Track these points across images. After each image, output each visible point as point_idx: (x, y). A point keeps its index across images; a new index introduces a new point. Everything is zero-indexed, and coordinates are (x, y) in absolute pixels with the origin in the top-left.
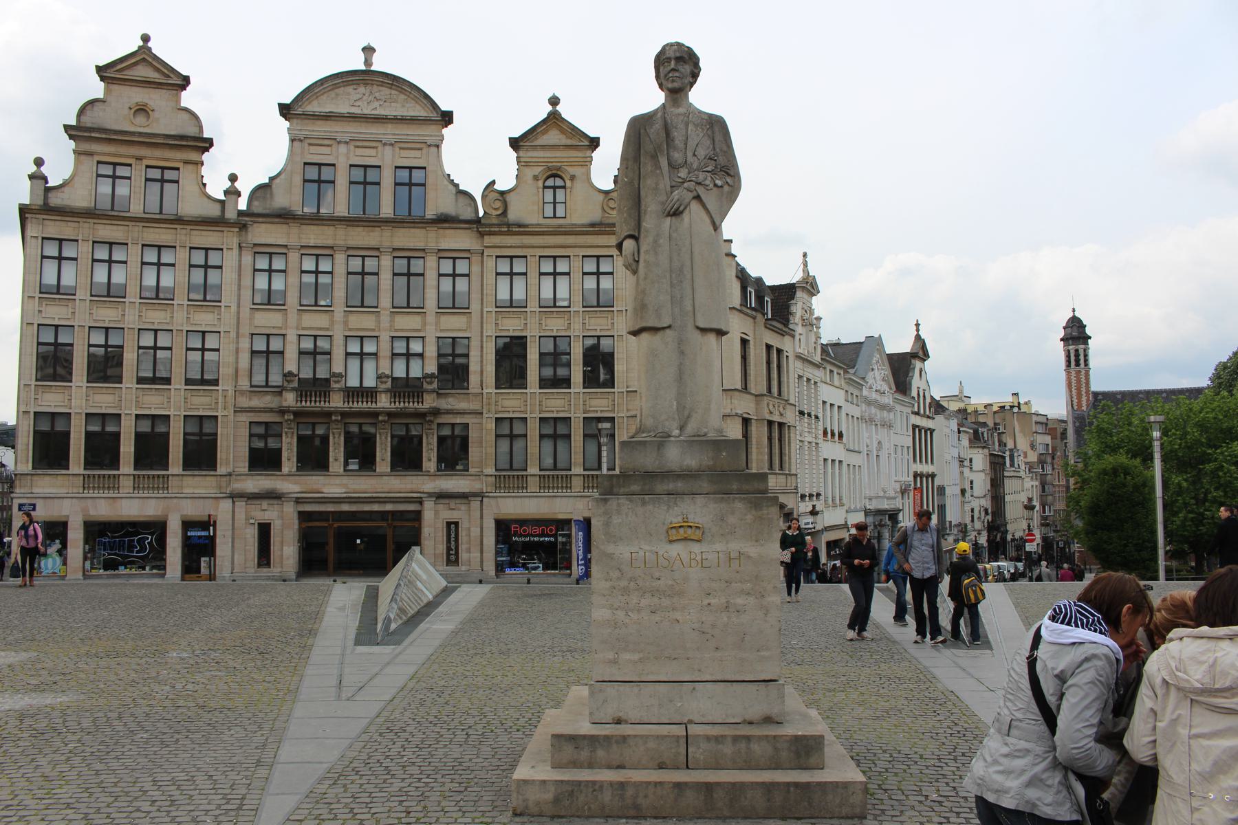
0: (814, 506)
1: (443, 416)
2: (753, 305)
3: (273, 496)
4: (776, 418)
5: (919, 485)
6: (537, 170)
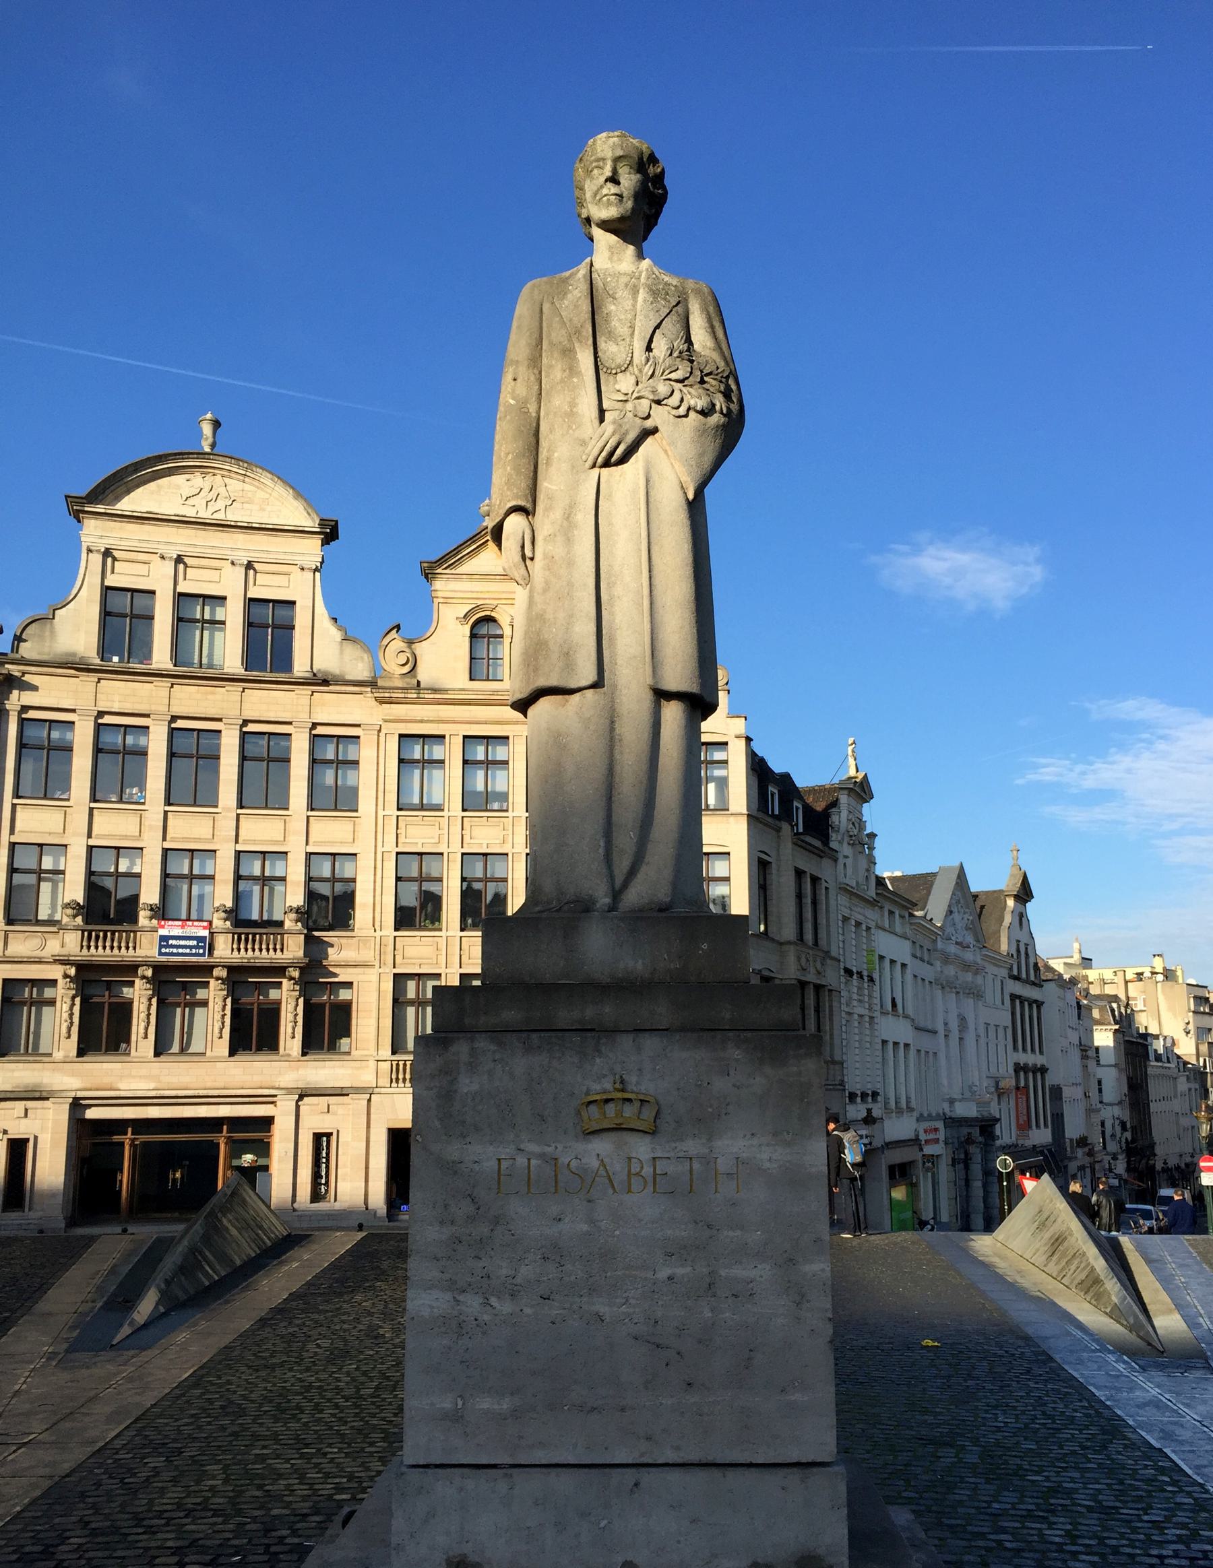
0: (869, 1111)
2: (777, 812)
4: (811, 977)
5: (1022, 1084)
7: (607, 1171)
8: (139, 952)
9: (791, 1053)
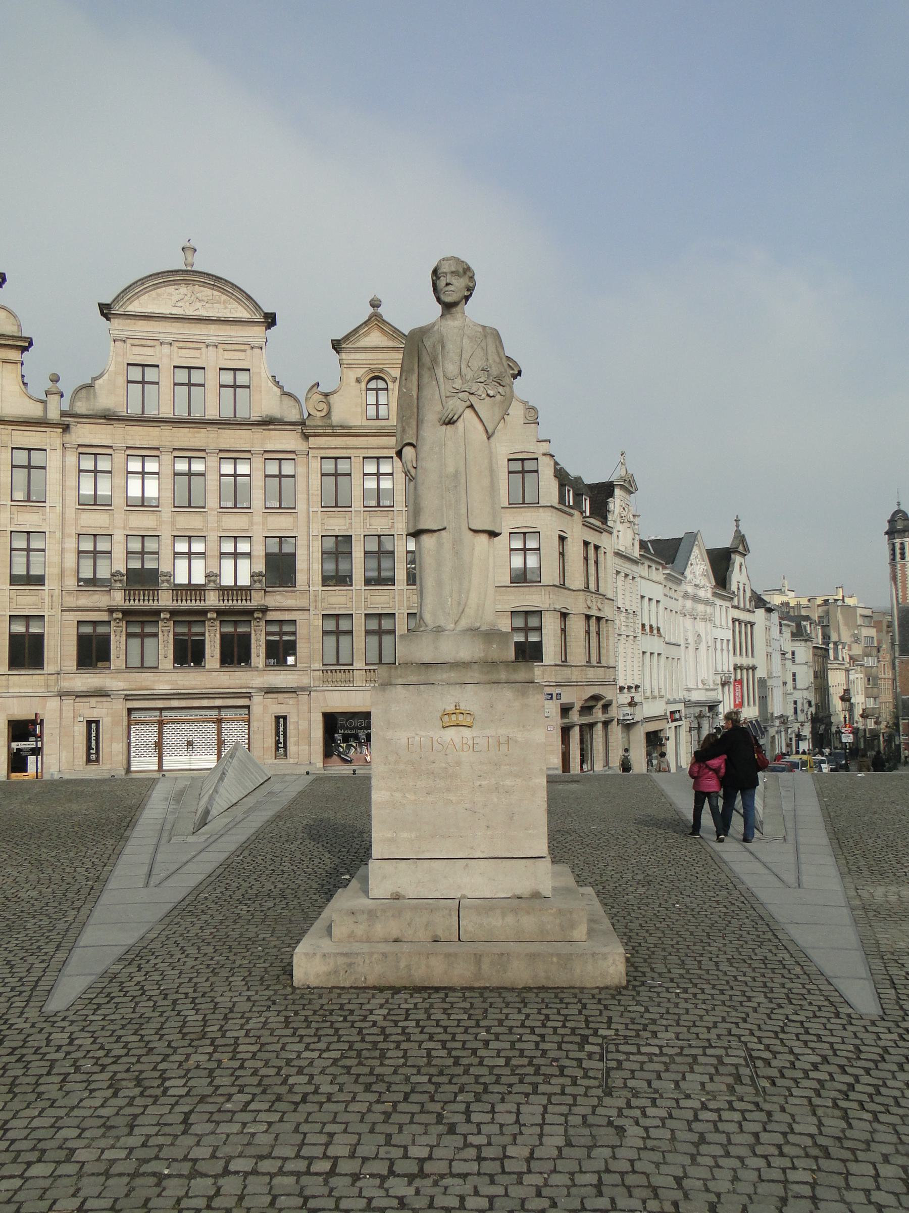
0: (632, 698)
1: (271, 613)
2: (571, 504)
3: (101, 694)
6: (360, 372)
8: (161, 603)
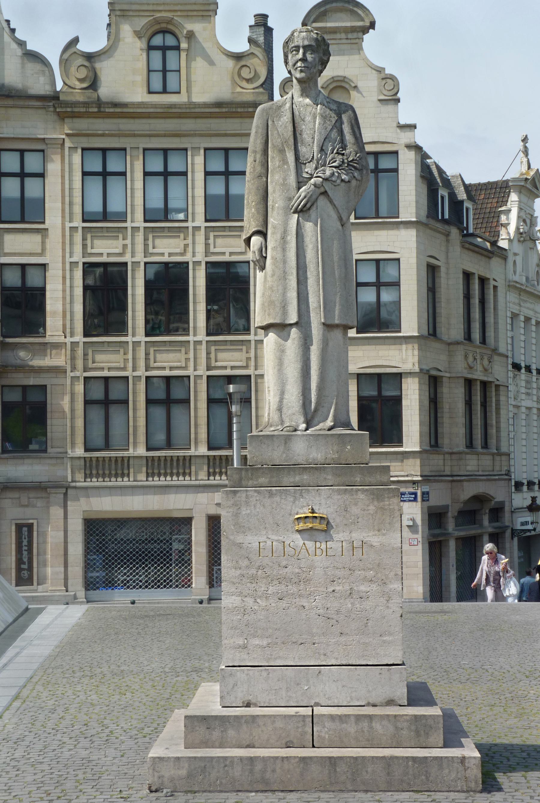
0: (534, 499)
2: (447, 216)
4: (478, 375)
7: (306, 547)
9: (386, 495)
